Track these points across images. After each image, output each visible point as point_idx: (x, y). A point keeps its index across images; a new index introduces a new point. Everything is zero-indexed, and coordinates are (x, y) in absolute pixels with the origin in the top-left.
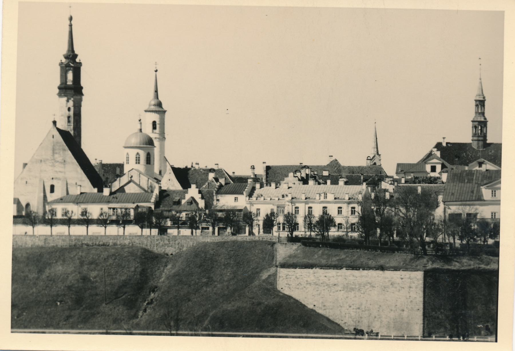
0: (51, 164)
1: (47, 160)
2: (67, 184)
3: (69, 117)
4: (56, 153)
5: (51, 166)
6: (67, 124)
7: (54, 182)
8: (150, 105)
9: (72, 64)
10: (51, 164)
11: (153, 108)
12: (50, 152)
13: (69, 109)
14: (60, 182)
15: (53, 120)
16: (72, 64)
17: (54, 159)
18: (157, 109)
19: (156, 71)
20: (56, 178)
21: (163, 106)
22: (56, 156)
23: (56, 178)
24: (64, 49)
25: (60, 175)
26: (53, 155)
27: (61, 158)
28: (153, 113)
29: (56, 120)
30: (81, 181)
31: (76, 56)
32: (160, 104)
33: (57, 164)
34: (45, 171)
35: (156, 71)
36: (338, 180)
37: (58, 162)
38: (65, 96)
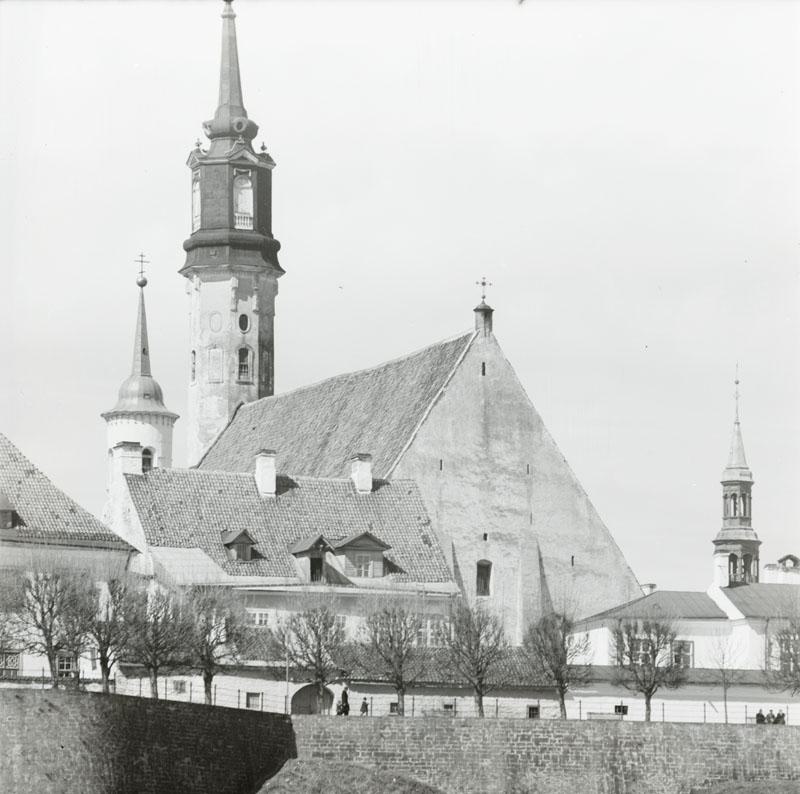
0: (477, 480)
1: (466, 460)
2: (541, 560)
3: (243, 353)
4: (497, 437)
5: (480, 487)
6: (236, 376)
7: (493, 554)
8: (123, 395)
9: (236, 161)
10: (477, 480)
11: (135, 404)
12: (473, 433)
13: (243, 322)
14: (515, 552)
15: (478, 303)
16: (236, 161)
17: (489, 460)
18: (151, 406)
19: (143, 284)
20: (498, 537)
21: (165, 400)
22: (498, 447)
23: (498, 537)
24: (208, 105)
25: (513, 525)
26: (486, 444)
27: (516, 458)
28: (132, 421)
29: (489, 303)
30: (590, 550)
31: (252, 131)
32: (156, 395)
33: (500, 480)
34: (458, 505)
35: (143, 284)
36: (214, 707)
37: (504, 470)
38: (231, 270)
